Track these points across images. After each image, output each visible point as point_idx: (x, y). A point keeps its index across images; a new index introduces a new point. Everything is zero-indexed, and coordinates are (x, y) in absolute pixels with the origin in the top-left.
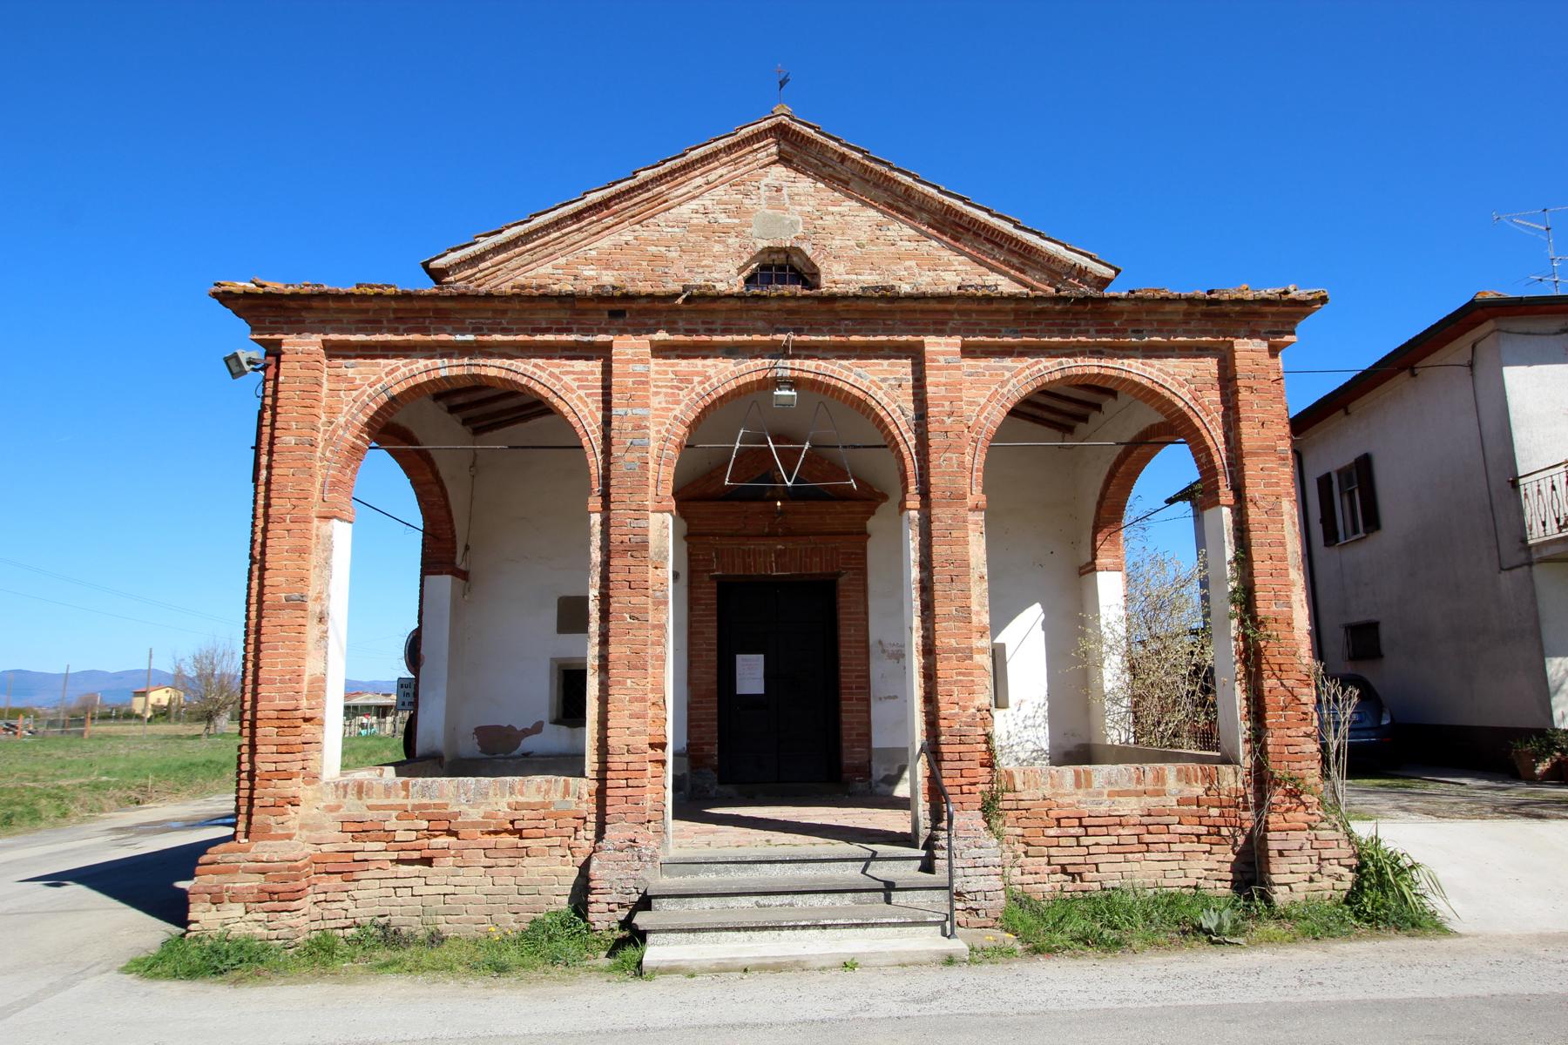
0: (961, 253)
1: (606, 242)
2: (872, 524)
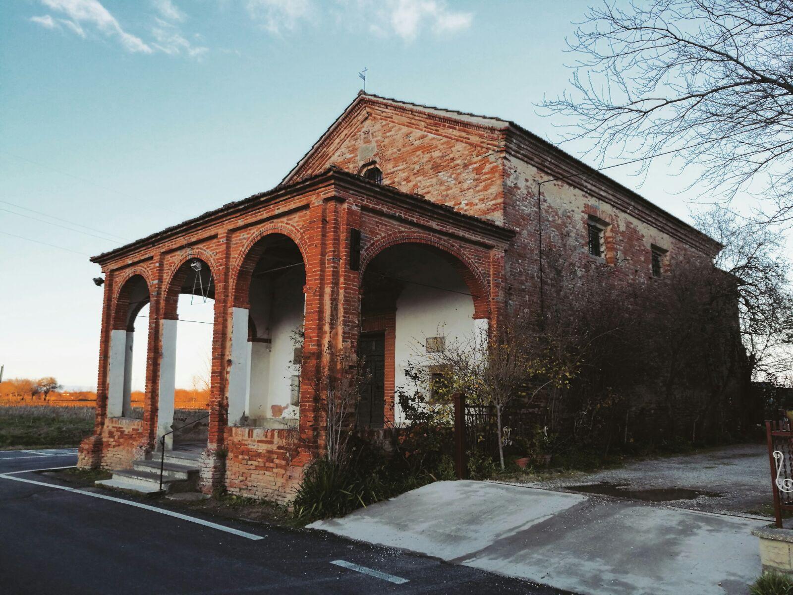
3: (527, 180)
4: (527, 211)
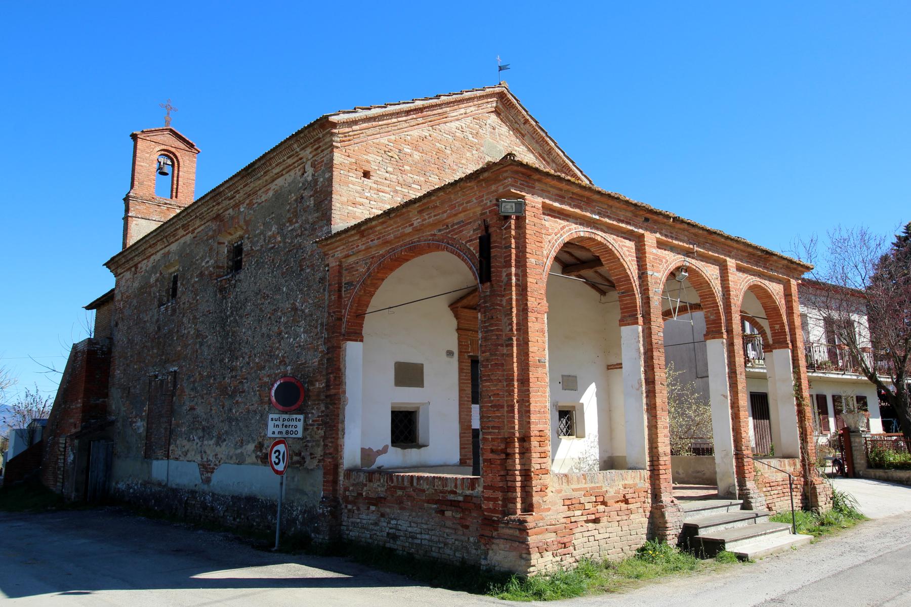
1: (416, 133)
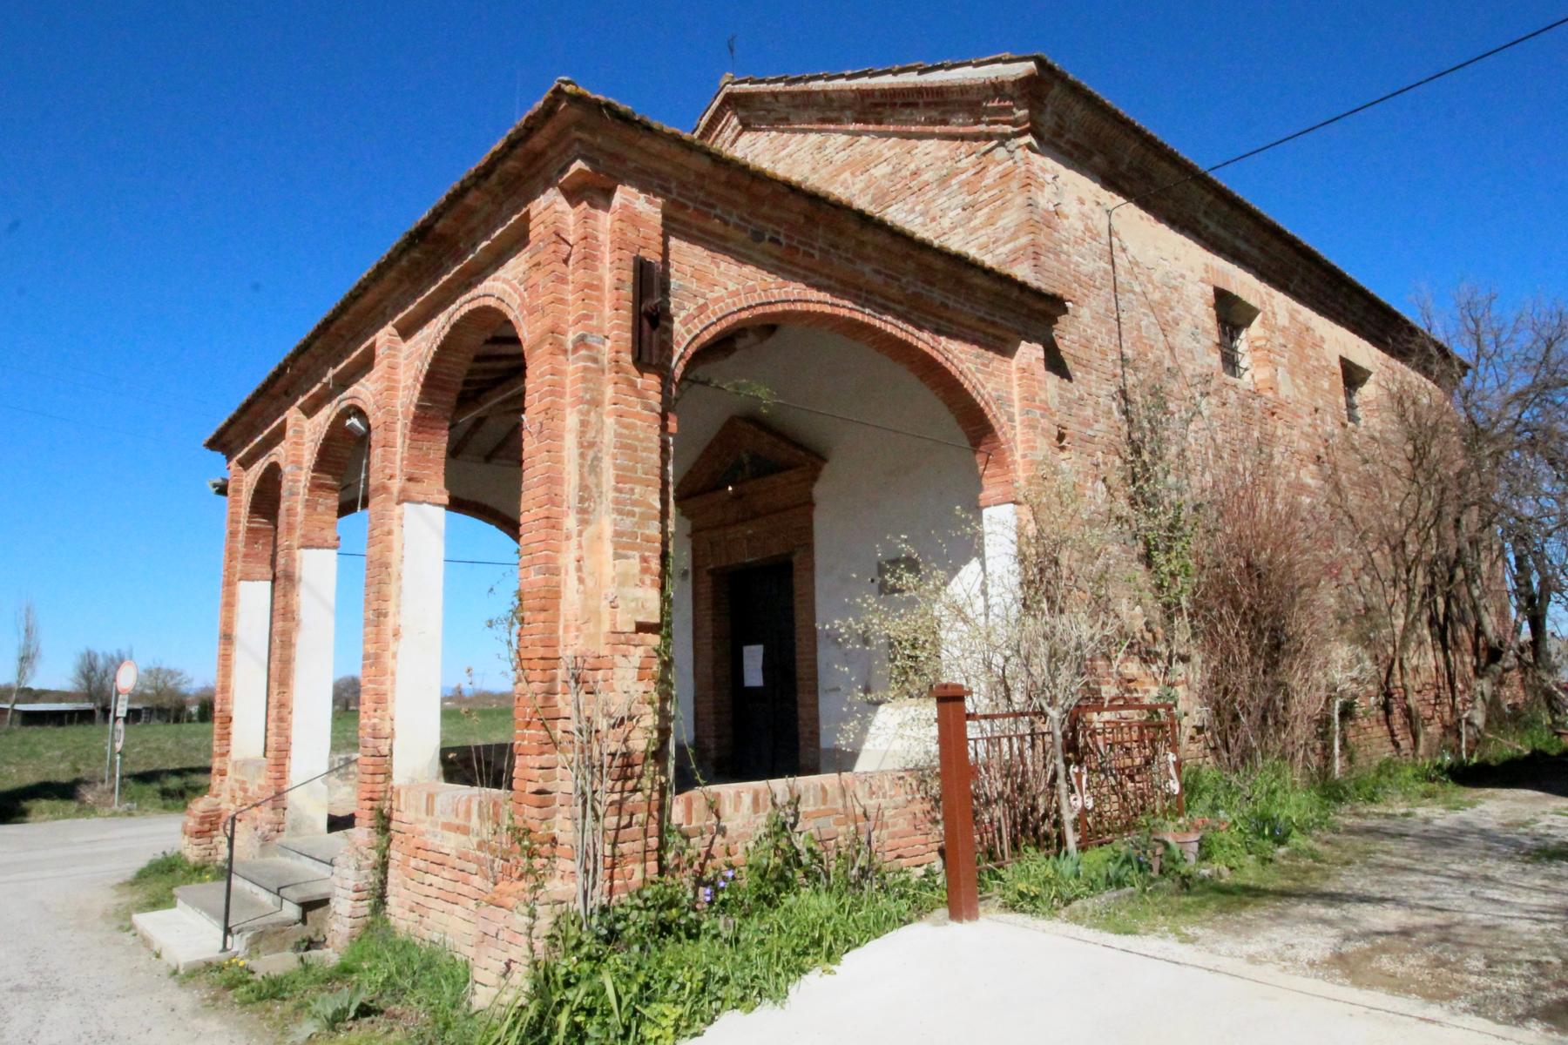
0: (888, 135)
2: (818, 490)
3: (1082, 202)
4: (1088, 266)
